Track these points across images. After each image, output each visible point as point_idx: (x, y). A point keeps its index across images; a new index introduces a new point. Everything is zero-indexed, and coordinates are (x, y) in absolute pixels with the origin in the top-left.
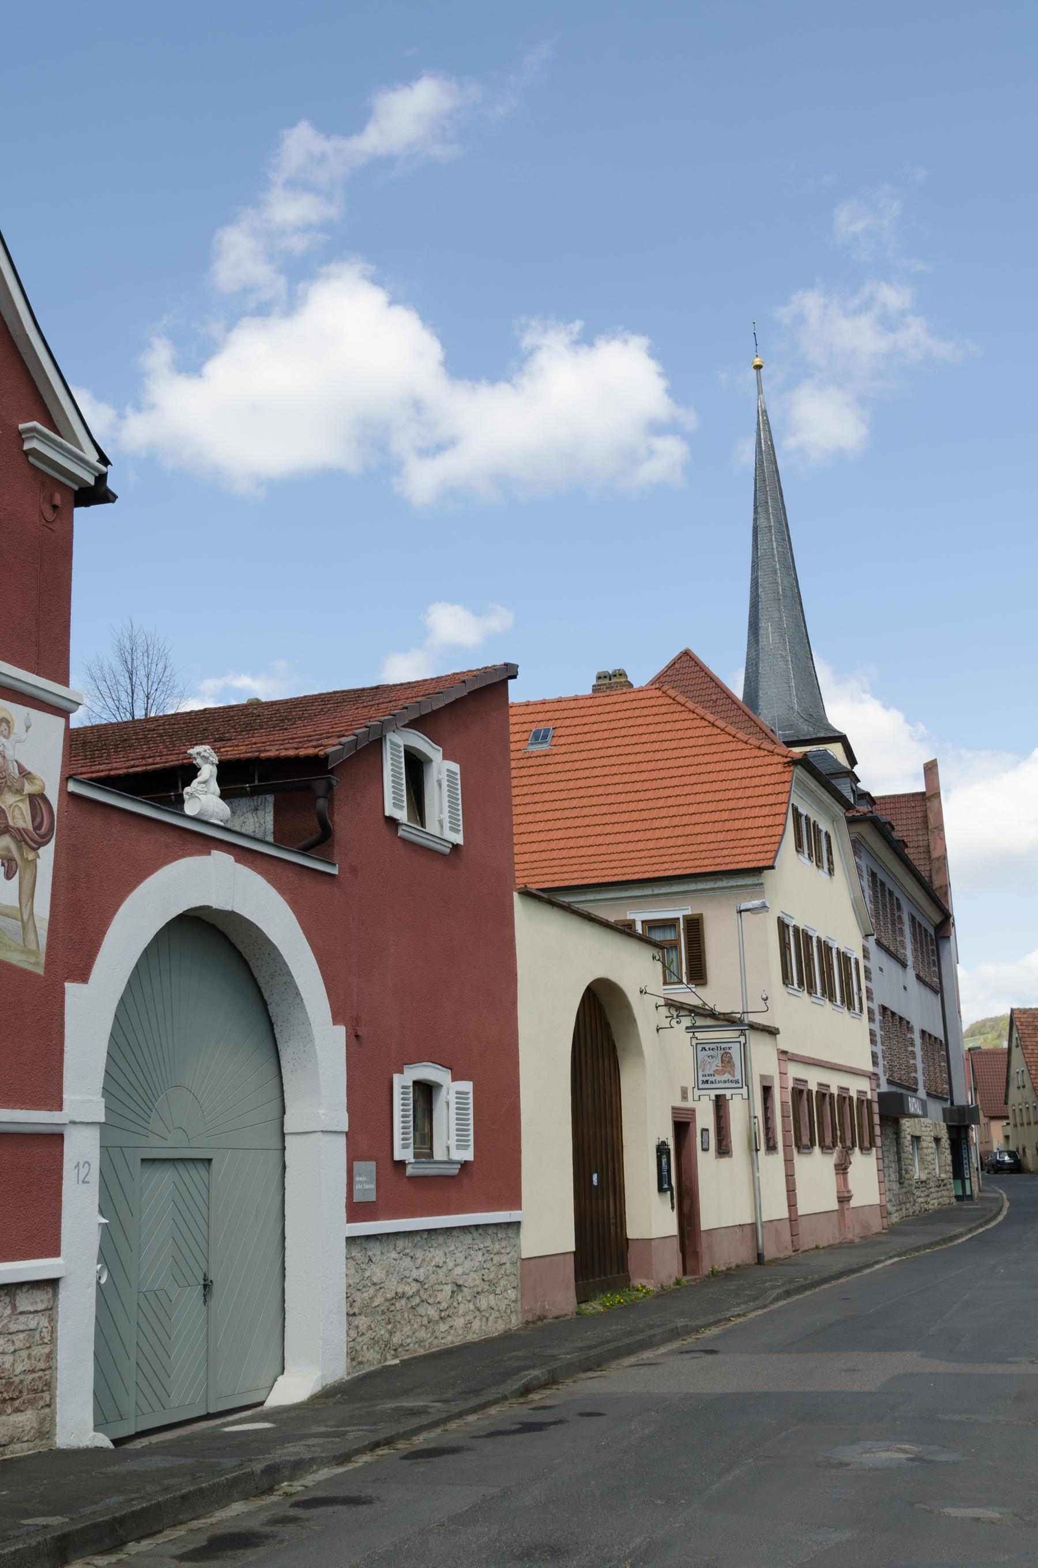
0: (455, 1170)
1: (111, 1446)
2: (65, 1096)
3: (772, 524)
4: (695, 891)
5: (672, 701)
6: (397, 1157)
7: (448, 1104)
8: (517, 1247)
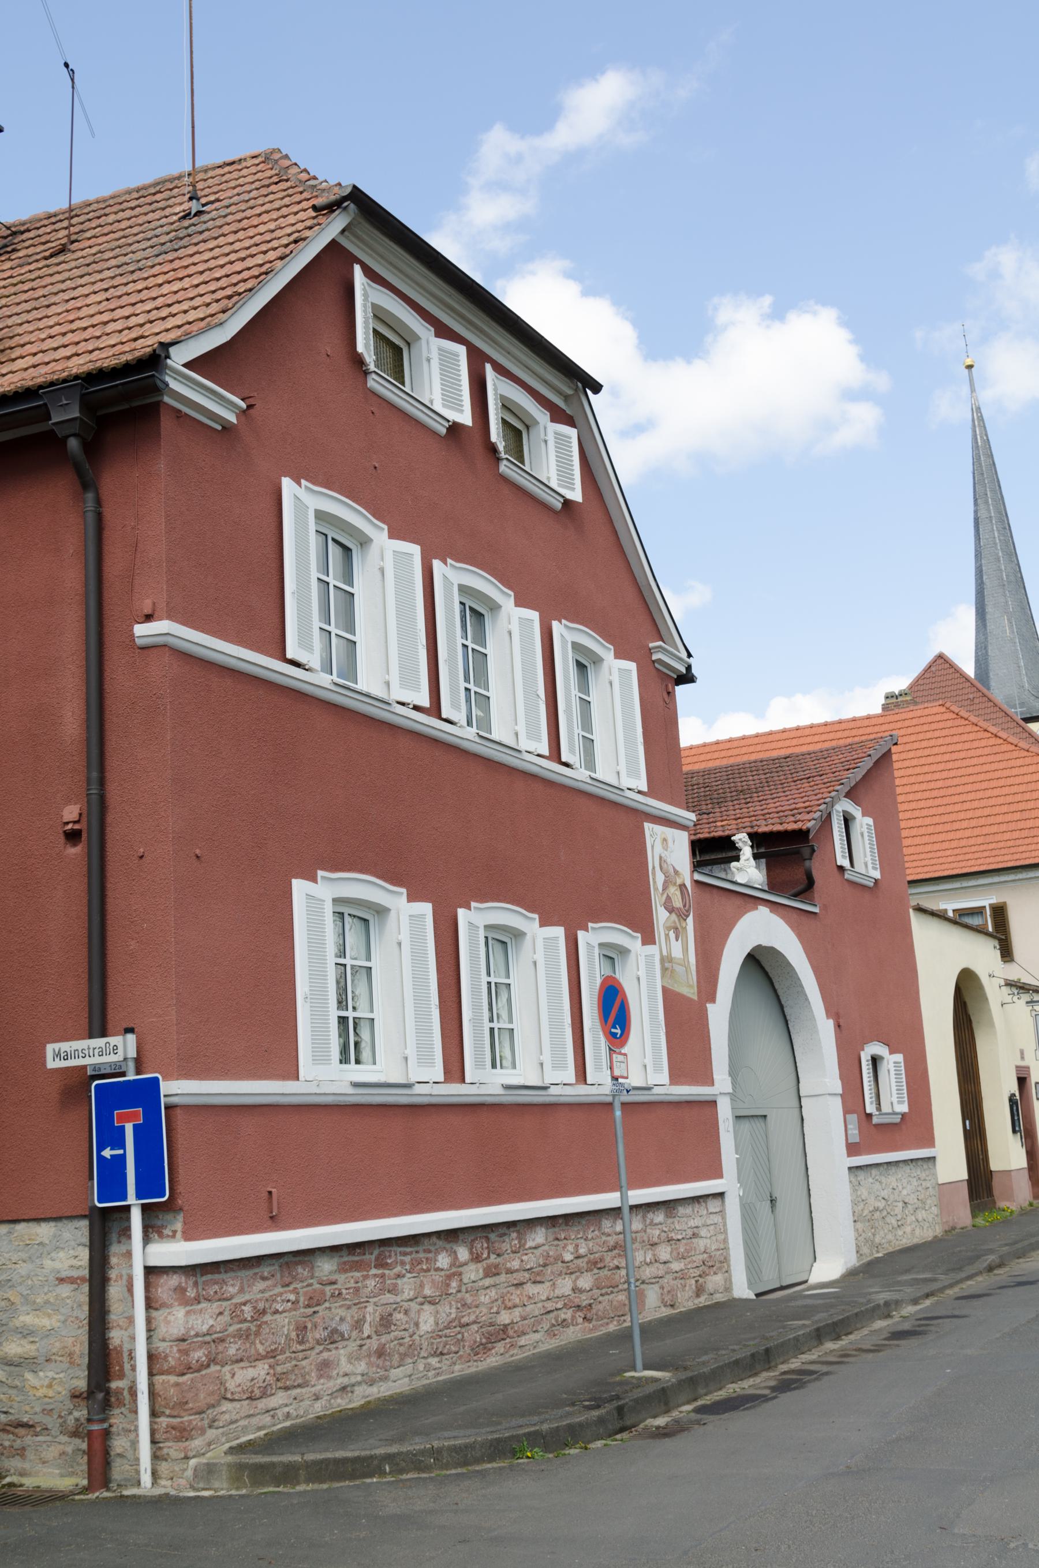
0: (897, 1119)
1: (754, 1297)
2: (715, 1077)
3: (993, 515)
4: (998, 883)
5: (955, 716)
6: (868, 1111)
7: (889, 1071)
8: (935, 1175)
